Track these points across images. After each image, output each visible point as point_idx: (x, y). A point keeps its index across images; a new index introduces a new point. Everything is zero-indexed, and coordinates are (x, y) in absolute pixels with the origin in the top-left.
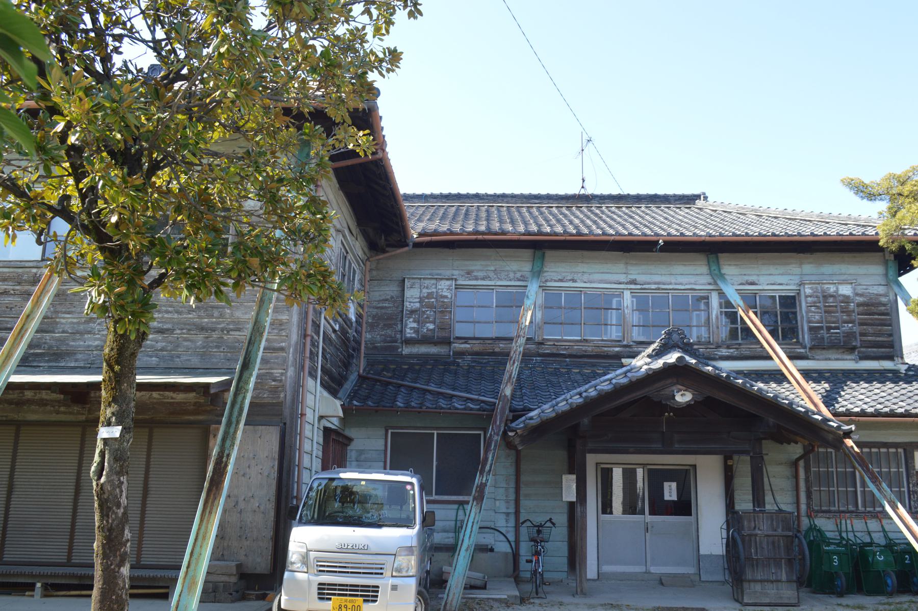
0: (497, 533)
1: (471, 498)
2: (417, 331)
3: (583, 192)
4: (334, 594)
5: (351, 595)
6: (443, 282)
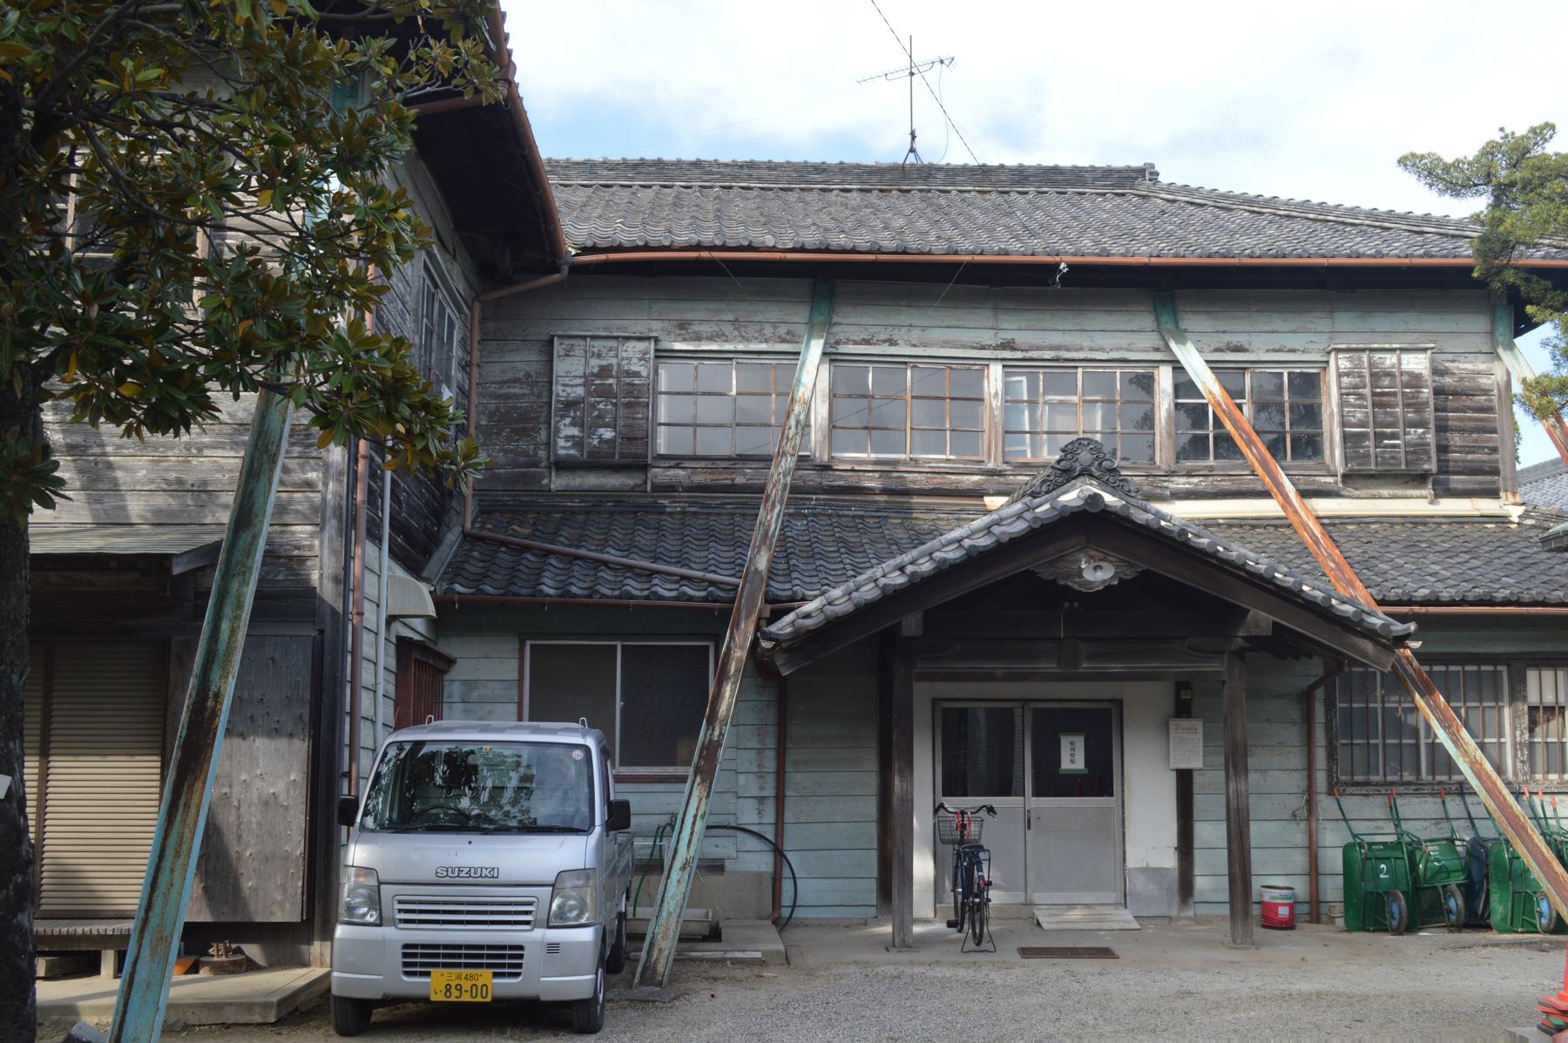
0: (741, 835)
1: (690, 771)
2: (578, 443)
3: (911, 159)
4: (436, 965)
5: (467, 965)
6: (631, 345)
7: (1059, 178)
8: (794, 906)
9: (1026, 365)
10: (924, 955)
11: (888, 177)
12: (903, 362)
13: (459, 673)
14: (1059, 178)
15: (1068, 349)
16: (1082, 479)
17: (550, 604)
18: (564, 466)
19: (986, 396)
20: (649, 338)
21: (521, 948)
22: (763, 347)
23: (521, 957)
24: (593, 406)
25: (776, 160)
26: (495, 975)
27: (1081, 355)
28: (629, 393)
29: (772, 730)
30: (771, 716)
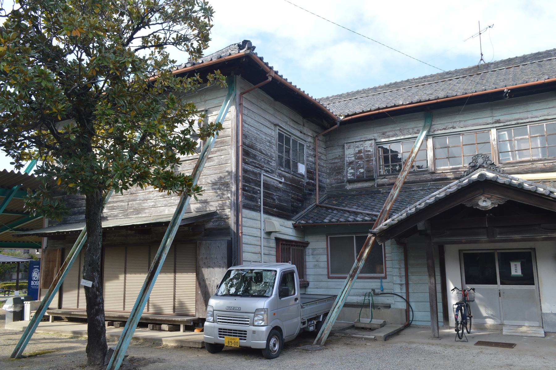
0: (395, 296)
1: (348, 276)
2: (353, 174)
3: (482, 62)
4: (226, 335)
5: (234, 336)
6: (367, 142)
7: (540, 56)
8: (412, 320)
9: (506, 127)
10: (444, 341)
11: (473, 71)
12: (459, 134)
13: (310, 246)
14: (540, 56)
15: (522, 119)
16: (480, 169)
17: (326, 225)
18: (350, 182)
19: (491, 141)
20: (372, 139)
21: (246, 331)
22: (410, 136)
23: (246, 334)
24: (357, 163)
25: (433, 74)
26: (240, 339)
27: (527, 120)
28: (368, 157)
29: (403, 262)
30: (402, 257)
